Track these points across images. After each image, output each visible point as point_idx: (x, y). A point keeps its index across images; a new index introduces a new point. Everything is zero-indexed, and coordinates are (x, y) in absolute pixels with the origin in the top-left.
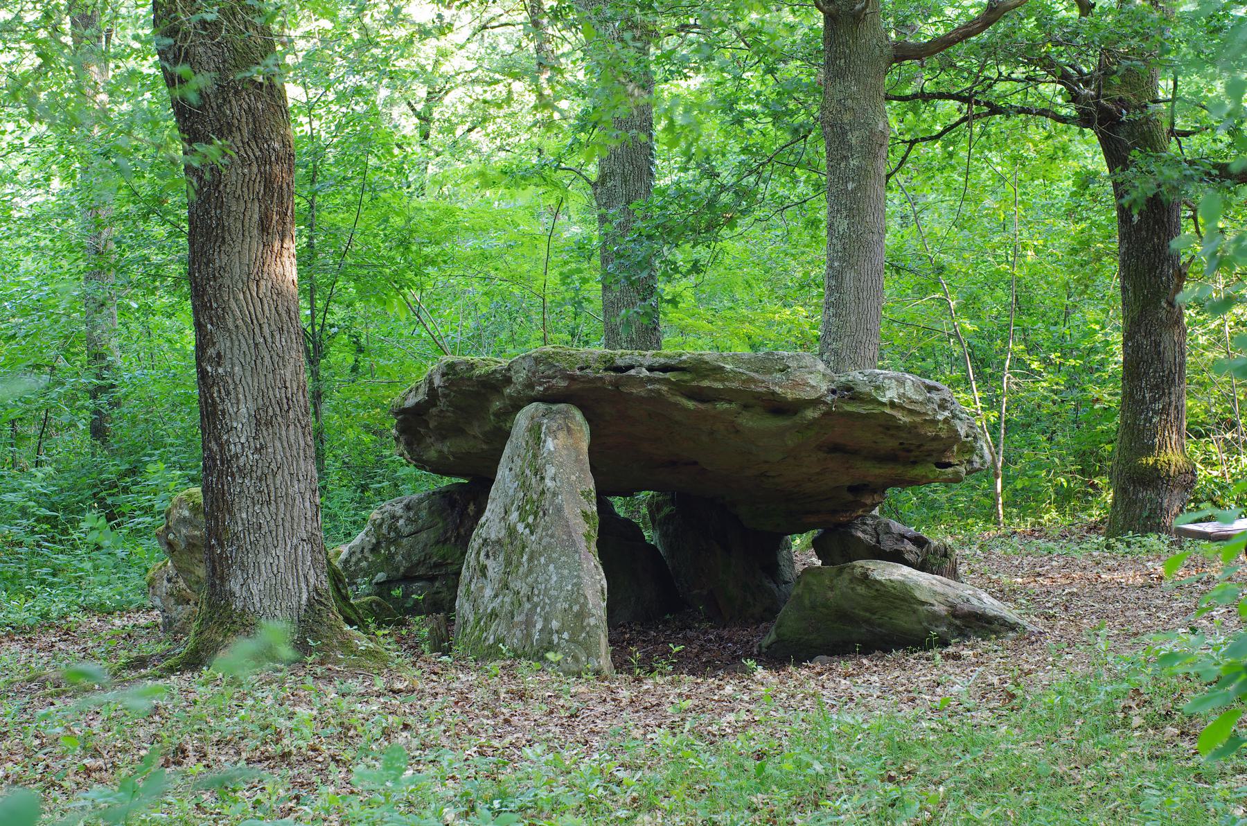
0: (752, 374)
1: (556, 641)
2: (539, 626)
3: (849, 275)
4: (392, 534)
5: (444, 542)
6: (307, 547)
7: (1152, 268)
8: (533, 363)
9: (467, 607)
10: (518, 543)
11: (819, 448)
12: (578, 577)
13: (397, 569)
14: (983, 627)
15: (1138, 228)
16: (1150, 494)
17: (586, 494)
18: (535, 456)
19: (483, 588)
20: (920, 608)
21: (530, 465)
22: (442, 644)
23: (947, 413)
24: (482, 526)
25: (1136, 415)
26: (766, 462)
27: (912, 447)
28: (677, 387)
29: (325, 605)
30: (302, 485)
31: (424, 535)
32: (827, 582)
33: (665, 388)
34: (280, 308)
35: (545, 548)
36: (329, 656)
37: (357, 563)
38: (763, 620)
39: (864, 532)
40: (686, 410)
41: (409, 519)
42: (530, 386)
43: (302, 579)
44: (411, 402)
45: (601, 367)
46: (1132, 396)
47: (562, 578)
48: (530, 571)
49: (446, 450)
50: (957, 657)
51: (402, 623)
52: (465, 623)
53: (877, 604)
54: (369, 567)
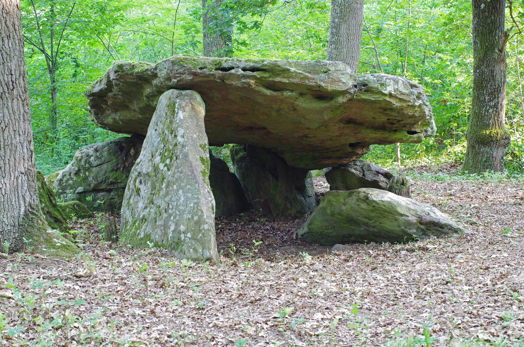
0: (307, 74)
1: (183, 238)
2: (172, 228)
3: (343, 27)
5: (117, 170)
6: (25, 178)
7: (491, 32)
8: (171, 64)
9: (128, 212)
10: (159, 176)
11: (341, 121)
12: (198, 198)
13: (90, 185)
14: (438, 230)
15: (484, 11)
16: (487, 149)
17: (203, 147)
18: (171, 122)
19: (137, 202)
20: (400, 218)
21: (168, 128)
22: (113, 236)
23: (420, 101)
24: (138, 164)
25: (480, 108)
26: (308, 128)
27: (395, 122)
28: (260, 81)
29: (36, 215)
30: (22, 138)
31: (105, 166)
32: (342, 200)
33: (252, 82)
34: (8, 23)
35: (177, 180)
36: (38, 248)
37: (66, 181)
38: (296, 217)
39: (355, 169)
40: (265, 95)
41: (97, 157)
42: (169, 79)
43: (21, 198)
44: (97, 89)
45: (214, 67)
46: (478, 98)
47: (187, 198)
48: (167, 194)
49: (117, 118)
50: (425, 249)
51: (91, 216)
52: (127, 222)
53: (373, 215)
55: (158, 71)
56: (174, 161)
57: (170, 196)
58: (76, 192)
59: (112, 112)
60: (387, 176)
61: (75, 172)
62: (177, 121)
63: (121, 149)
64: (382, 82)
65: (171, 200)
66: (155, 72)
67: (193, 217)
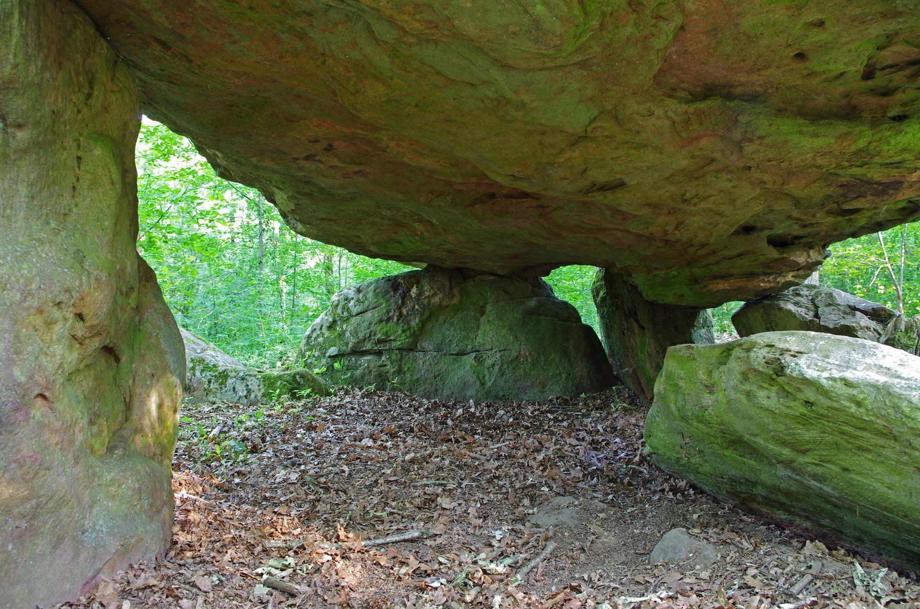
4: (345, 314)
32: (702, 375)
37: (316, 339)
39: (796, 304)
41: (358, 300)
53: (808, 435)
54: (324, 342)
58: (327, 355)
60: (879, 315)
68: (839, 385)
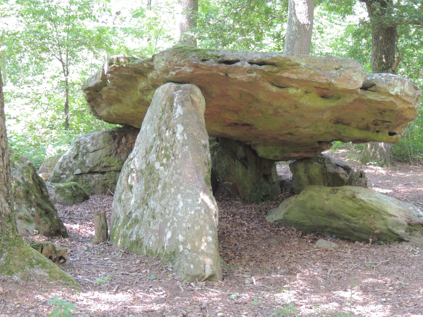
5: (110, 155)
20: (389, 218)
31: (100, 152)
35: (175, 182)
41: (93, 143)
42: (166, 71)
44: (91, 84)
47: (186, 204)
48: (163, 196)
53: (359, 212)
55: (155, 63)
56: (172, 160)
57: (167, 200)
58: (75, 174)
59: (107, 105)
61: (74, 156)
62: (176, 117)
63: (115, 138)
64: (391, 82)
65: (167, 204)
66: (152, 64)
67: (194, 227)
68: (369, 201)
